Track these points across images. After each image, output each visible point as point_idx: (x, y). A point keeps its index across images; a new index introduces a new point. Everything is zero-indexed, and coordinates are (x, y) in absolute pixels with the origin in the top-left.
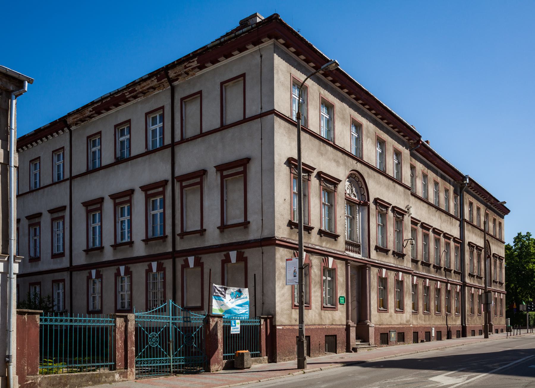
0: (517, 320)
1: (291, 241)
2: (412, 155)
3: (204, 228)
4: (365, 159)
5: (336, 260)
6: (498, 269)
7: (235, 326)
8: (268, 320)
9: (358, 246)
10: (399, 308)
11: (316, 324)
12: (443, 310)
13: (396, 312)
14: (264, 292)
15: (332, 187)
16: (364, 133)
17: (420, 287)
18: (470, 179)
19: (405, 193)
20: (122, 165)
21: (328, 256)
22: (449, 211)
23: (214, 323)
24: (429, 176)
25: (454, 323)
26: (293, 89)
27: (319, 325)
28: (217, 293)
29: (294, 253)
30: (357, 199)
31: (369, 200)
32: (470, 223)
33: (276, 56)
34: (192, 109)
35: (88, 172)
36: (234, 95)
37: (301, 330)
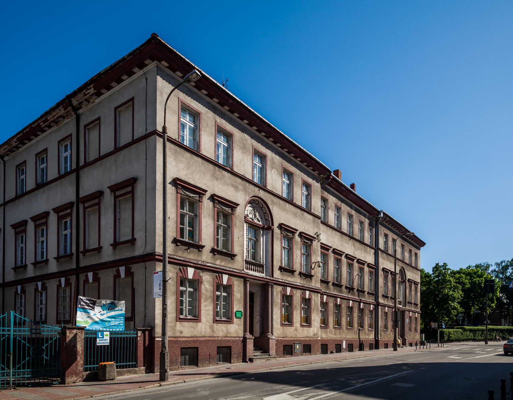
0: (431, 336)
1: (175, 257)
2: (323, 188)
3: (101, 245)
4: (269, 187)
5: (231, 277)
6: (413, 293)
7: (103, 337)
8: (147, 333)
9: (262, 266)
10: (307, 322)
11: (207, 335)
12: (356, 325)
13: (302, 326)
14: (147, 305)
15: (229, 210)
16: (269, 163)
17: (331, 305)
18: (384, 214)
19: (314, 222)
20: (41, 190)
22: (363, 240)
23: (72, 335)
24: (343, 208)
25: (367, 337)
27: (210, 337)
28: (82, 305)
29: (180, 269)
30: (261, 223)
31: (273, 225)
32: (385, 252)
33: (159, 79)
34: (94, 135)
35: (17, 197)
36: (125, 119)
37: (360, 340)
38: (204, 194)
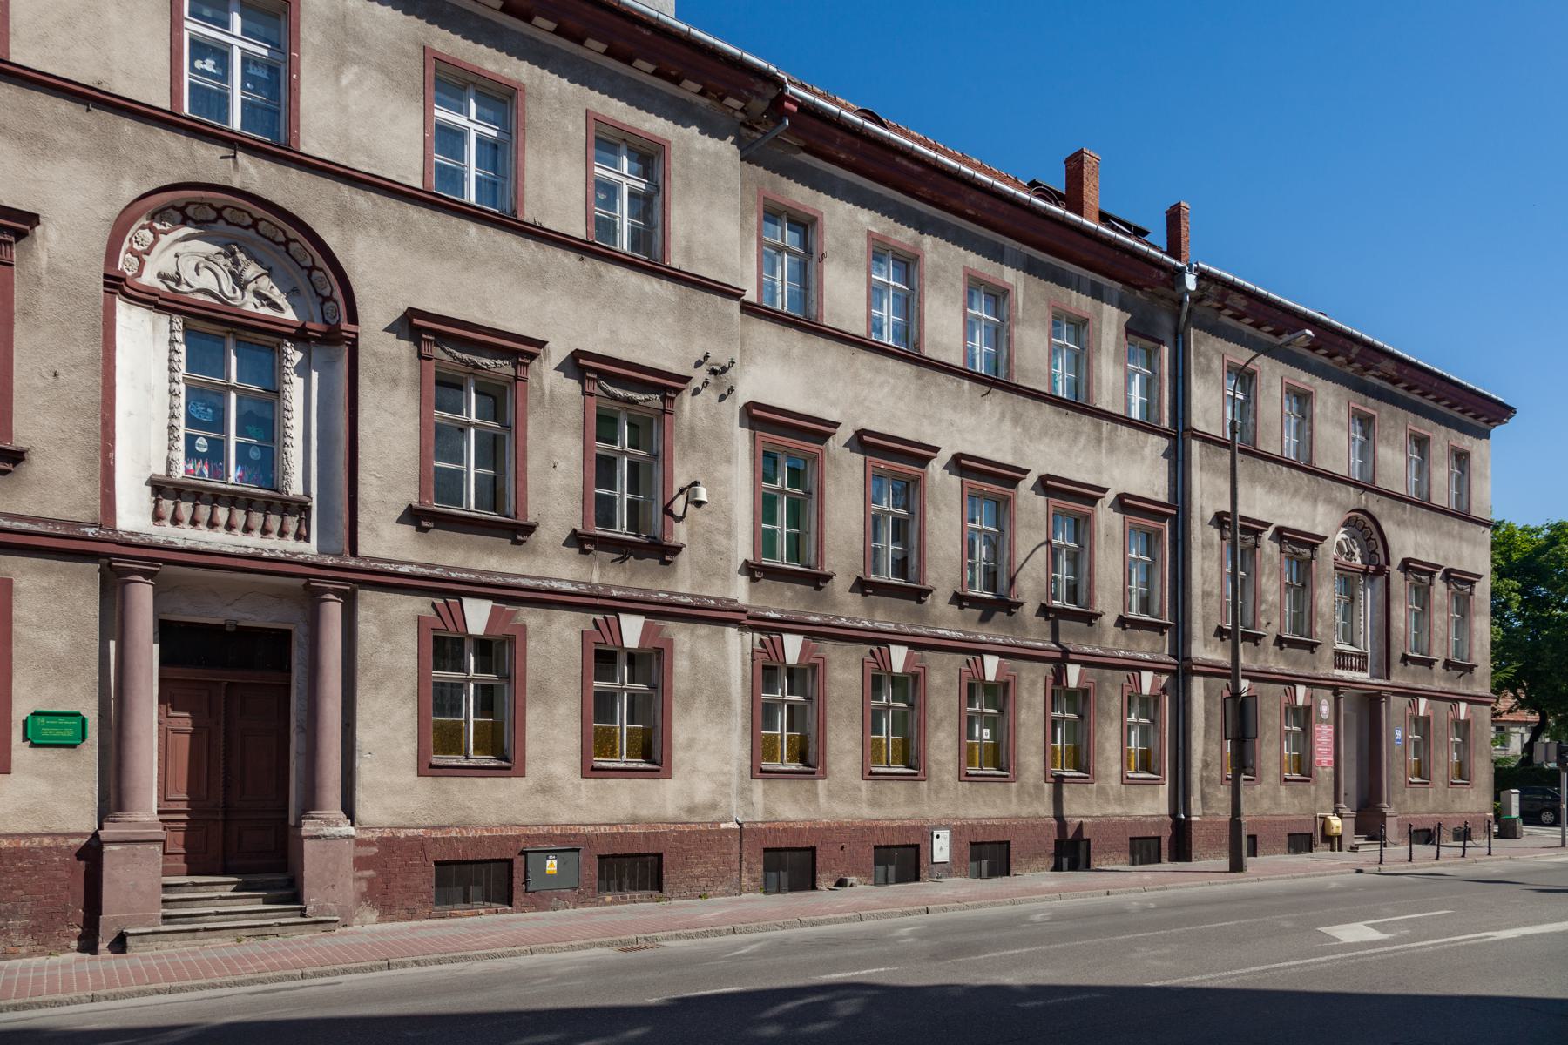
9: (300, 508)
21: (1458, 701)
26: (1227, 382)
29: (434, 605)
30: (290, 315)
31: (1388, 563)
38: (533, 356)
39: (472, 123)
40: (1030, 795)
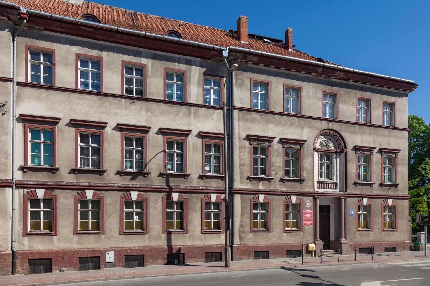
29: (78, 193)
39: (260, 91)
40: (155, 238)
